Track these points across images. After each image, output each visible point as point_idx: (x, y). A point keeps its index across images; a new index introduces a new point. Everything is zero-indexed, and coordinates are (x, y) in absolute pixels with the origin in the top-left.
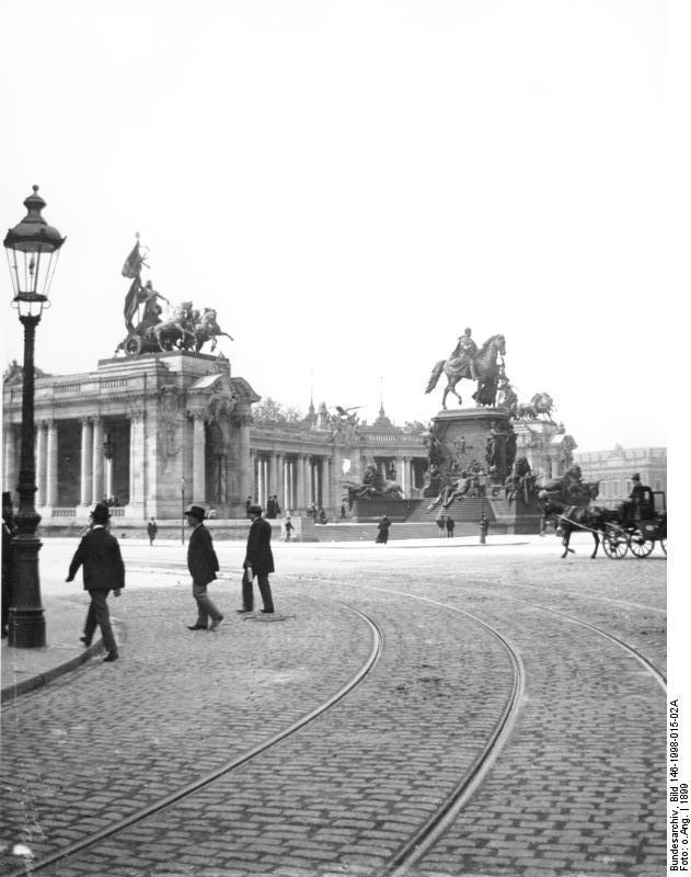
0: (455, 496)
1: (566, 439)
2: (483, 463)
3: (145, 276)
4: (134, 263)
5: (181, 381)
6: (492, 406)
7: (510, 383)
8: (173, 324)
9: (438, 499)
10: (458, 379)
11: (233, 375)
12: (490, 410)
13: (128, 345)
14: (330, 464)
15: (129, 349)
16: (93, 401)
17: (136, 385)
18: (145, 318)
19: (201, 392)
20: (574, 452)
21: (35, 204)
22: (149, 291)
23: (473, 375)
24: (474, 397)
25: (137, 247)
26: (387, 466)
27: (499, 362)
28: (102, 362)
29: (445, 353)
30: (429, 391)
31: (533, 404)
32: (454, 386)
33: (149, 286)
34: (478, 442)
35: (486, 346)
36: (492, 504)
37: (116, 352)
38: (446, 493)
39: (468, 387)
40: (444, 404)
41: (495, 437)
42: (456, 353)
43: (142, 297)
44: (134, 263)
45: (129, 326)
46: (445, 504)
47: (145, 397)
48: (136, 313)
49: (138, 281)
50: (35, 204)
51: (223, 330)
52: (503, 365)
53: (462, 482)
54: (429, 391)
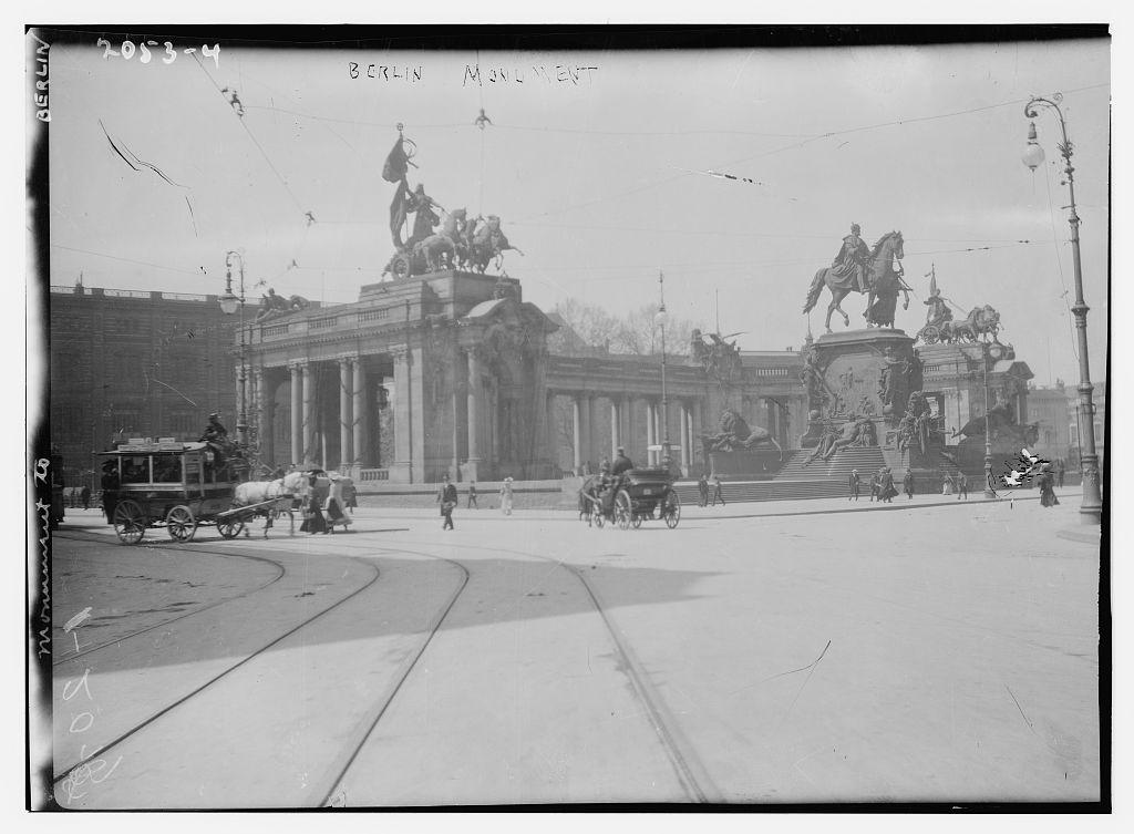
0: (838, 445)
1: (1016, 365)
2: (876, 399)
3: (413, 178)
4: (397, 165)
5: (450, 310)
6: (890, 327)
7: (942, 295)
8: (443, 239)
9: (817, 449)
10: (844, 293)
11: (524, 300)
12: (886, 331)
13: (394, 267)
14: (702, 408)
15: (396, 272)
16: (354, 339)
17: (397, 317)
18: (415, 231)
19: (475, 322)
20: (1030, 383)
21: (483, 112)
22: (419, 197)
23: (861, 287)
24: (865, 315)
25: (401, 141)
26: (781, 406)
27: (896, 268)
28: (365, 289)
29: (826, 257)
30: (808, 310)
31: (970, 322)
32: (839, 302)
33: (421, 189)
34: (869, 366)
35: (879, 247)
36: (885, 453)
37: (383, 275)
38: (827, 442)
39: (857, 303)
40: (828, 326)
41: (890, 366)
42: (840, 259)
43: (410, 207)
44: (397, 165)
45: (397, 241)
46: (824, 456)
47: (407, 331)
48: (404, 225)
49: (404, 187)
50: (483, 112)
51: (510, 243)
52: (902, 270)
53: (849, 427)
54: (808, 310)
